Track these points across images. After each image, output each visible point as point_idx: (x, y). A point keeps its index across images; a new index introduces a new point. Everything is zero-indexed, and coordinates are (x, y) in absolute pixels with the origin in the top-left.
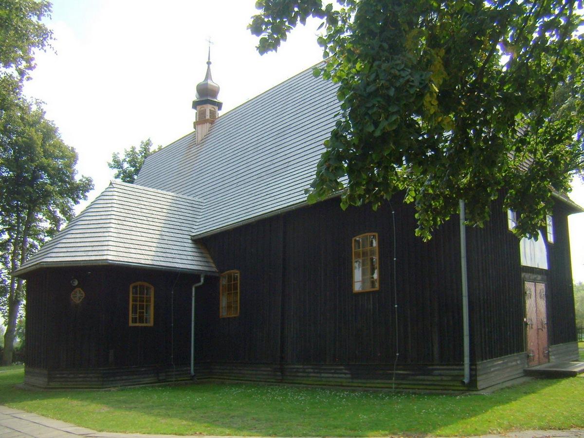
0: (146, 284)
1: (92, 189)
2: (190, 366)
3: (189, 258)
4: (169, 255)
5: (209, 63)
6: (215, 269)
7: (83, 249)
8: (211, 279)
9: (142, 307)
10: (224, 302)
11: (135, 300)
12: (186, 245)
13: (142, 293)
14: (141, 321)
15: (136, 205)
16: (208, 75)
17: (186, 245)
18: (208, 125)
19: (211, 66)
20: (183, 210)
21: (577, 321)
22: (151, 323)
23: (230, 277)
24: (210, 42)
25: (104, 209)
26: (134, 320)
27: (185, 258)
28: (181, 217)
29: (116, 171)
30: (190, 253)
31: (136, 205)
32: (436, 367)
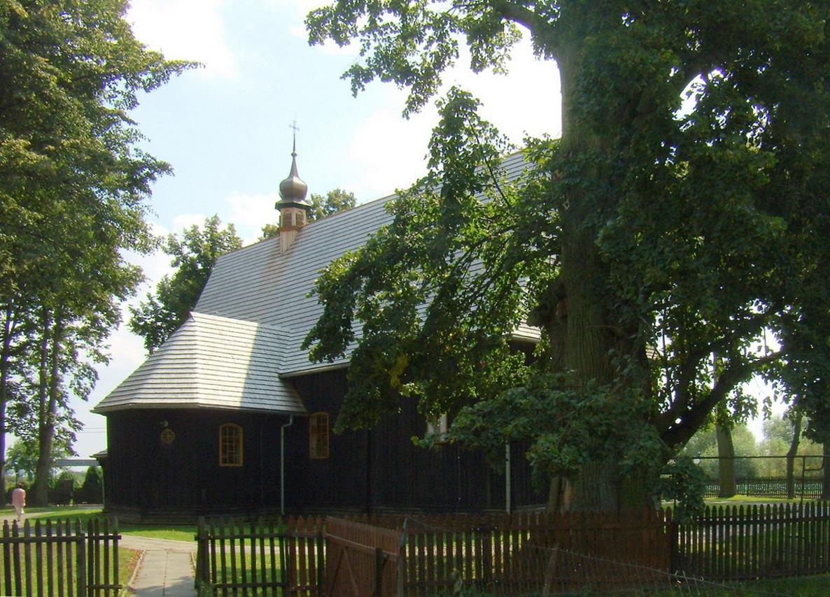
0: (235, 425)
1: (141, 281)
2: (280, 507)
3: (278, 398)
4: (257, 396)
5: (294, 155)
6: (304, 410)
7: (171, 391)
8: (301, 421)
9: (231, 447)
10: (313, 443)
11: (224, 441)
12: (273, 384)
13: (231, 434)
14: (231, 462)
15: (219, 341)
16: (294, 171)
17: (273, 384)
18: (294, 233)
19: (296, 158)
20: (269, 344)
21: (799, 447)
22: (241, 464)
23: (319, 417)
24: (294, 128)
25: (187, 347)
26: (225, 461)
27: (274, 400)
28: (268, 352)
29: (173, 258)
30: (278, 393)
31: (219, 341)
32: (718, 531)
